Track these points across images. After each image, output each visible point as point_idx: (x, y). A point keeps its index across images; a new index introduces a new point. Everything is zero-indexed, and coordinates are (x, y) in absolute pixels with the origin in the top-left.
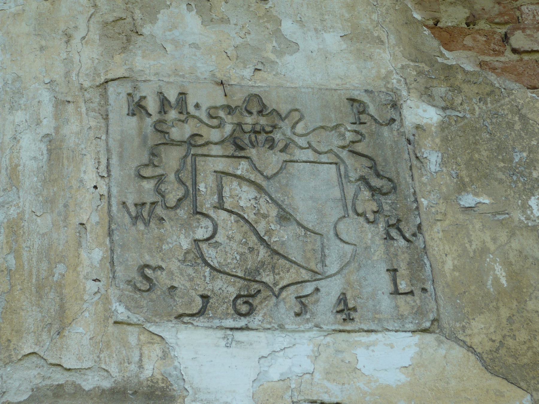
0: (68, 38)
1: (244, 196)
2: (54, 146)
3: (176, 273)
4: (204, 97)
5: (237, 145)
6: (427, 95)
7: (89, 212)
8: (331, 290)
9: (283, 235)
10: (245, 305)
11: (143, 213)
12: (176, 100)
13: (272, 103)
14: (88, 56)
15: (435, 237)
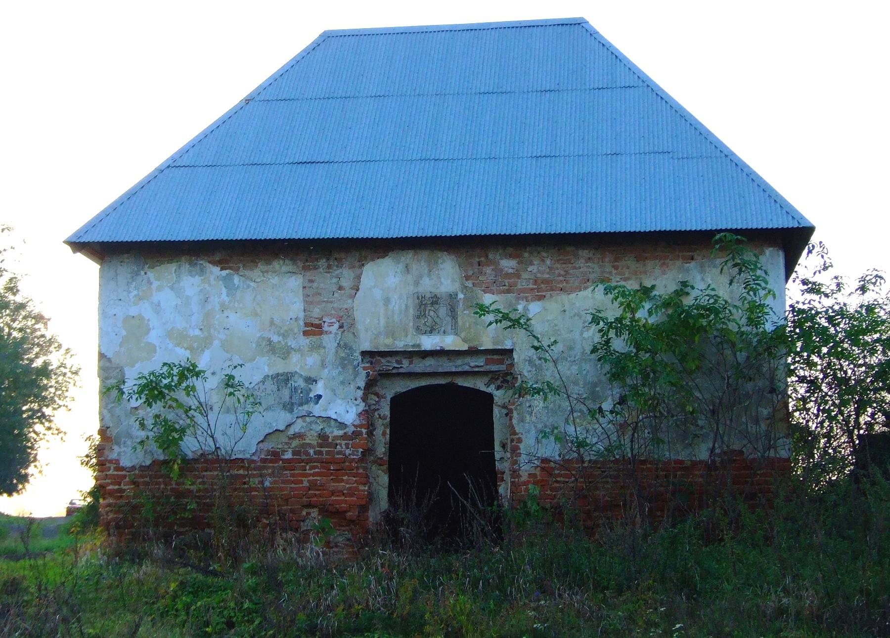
0: (229, 383)
1: (432, 313)
2: (406, 306)
3: (422, 327)
4: (428, 295)
5: (432, 304)
6: (462, 292)
7: (411, 318)
8: (443, 329)
9: (437, 320)
10: (431, 332)
11: (418, 317)
12: (383, 257)
13: (439, 296)
14: (412, 288)
15: (459, 319)
